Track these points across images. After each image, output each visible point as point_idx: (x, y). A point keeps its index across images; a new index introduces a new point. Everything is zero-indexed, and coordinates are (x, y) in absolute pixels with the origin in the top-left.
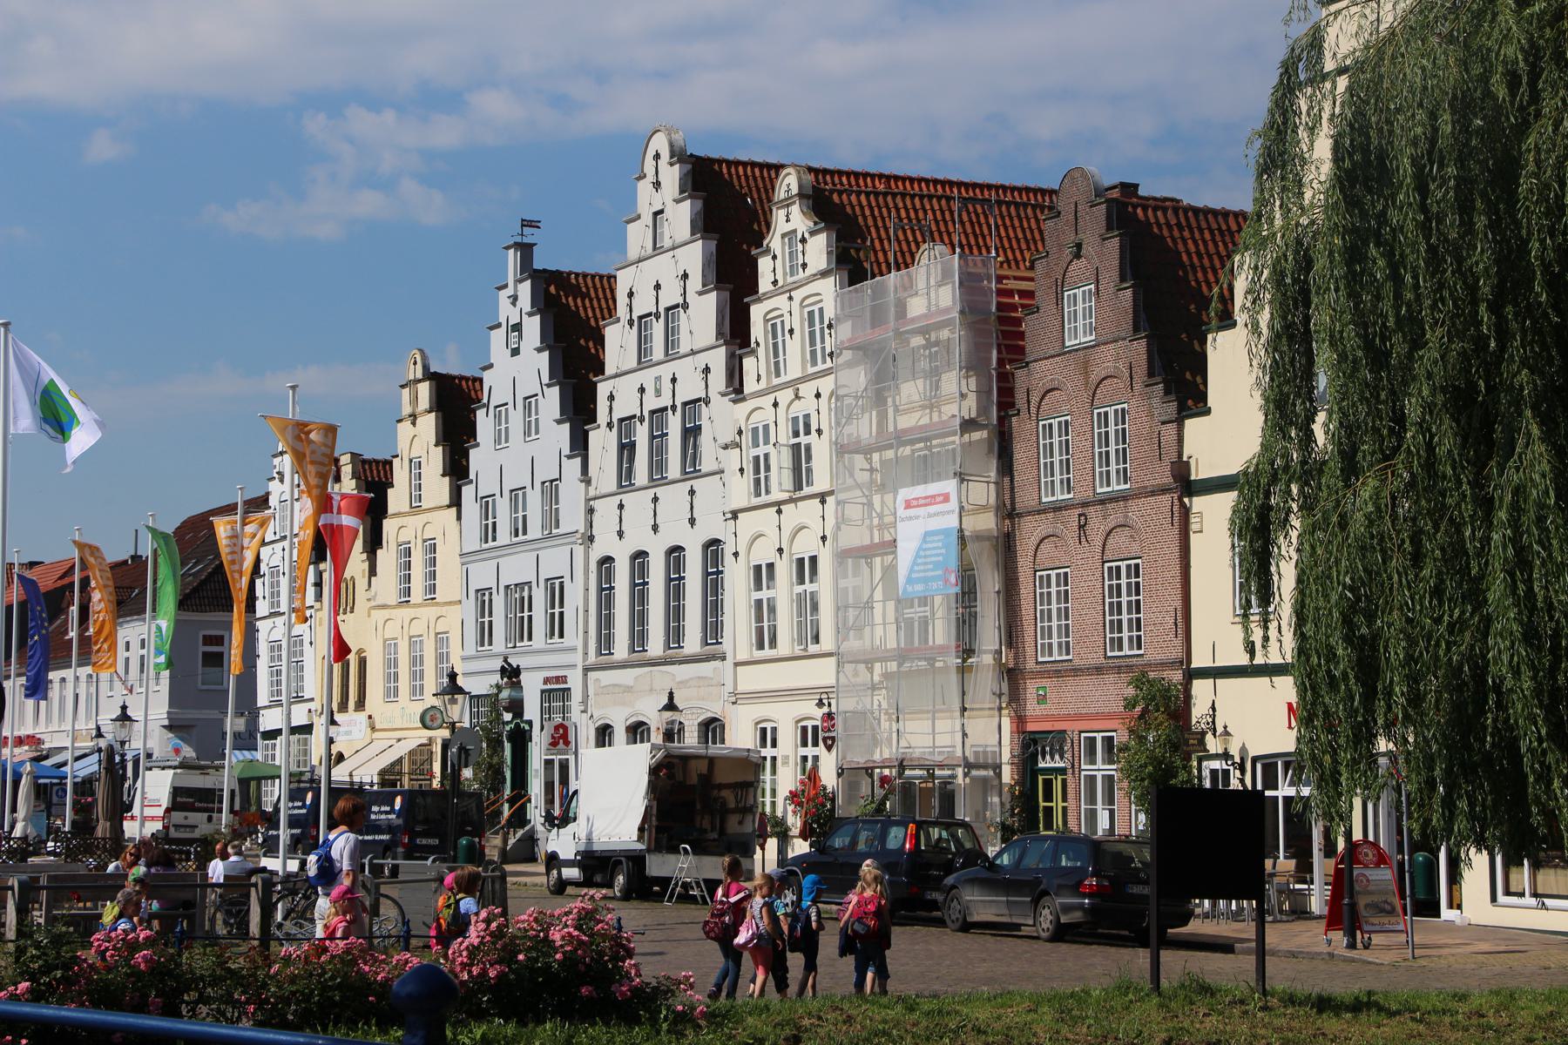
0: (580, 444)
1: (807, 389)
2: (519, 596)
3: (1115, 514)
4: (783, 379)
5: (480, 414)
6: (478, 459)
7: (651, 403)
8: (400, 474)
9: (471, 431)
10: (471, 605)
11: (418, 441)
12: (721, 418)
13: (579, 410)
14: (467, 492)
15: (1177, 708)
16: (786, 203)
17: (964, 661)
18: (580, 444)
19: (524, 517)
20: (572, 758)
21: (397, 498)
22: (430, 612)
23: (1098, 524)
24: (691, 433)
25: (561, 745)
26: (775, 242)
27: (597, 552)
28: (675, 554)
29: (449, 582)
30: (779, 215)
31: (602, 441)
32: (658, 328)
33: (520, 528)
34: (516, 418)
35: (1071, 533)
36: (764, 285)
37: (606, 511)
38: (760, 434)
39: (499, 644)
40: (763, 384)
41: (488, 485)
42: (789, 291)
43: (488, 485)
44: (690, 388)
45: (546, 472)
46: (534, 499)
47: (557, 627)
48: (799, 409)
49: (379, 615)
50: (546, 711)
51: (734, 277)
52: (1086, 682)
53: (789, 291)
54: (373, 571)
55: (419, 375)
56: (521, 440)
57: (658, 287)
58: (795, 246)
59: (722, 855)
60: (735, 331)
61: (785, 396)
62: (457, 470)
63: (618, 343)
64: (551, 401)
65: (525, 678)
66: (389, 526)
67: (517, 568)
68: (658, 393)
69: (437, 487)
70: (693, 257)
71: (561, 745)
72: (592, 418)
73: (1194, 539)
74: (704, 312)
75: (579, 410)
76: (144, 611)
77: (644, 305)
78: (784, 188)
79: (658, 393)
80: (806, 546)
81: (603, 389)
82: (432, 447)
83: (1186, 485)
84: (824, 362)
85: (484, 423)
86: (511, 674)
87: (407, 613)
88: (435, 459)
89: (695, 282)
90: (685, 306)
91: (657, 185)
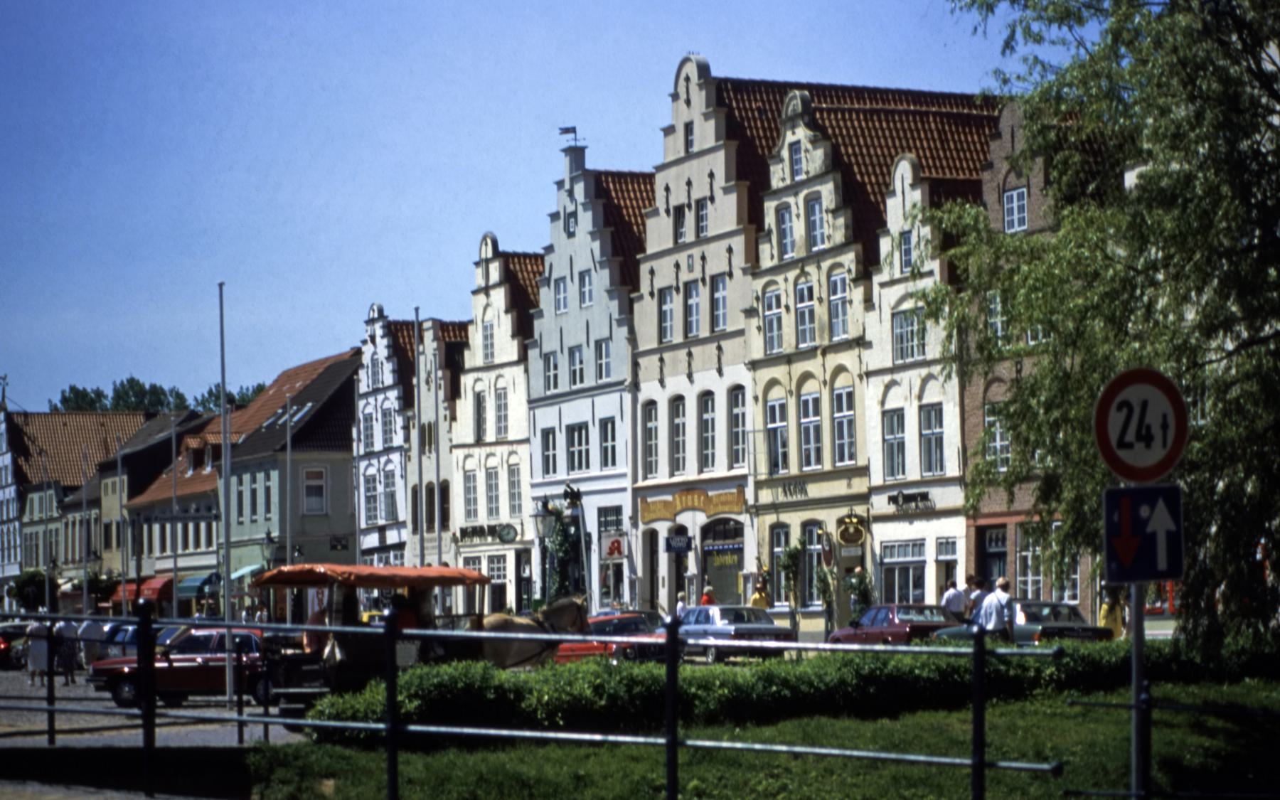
0: (627, 315)
2: (577, 431)
4: (770, 519)
6: (541, 326)
7: (685, 276)
8: (476, 337)
10: (537, 441)
11: (494, 312)
13: (626, 279)
14: (533, 353)
16: (792, 122)
17: (1232, 144)
18: (627, 315)
19: (581, 370)
20: (625, 562)
21: (473, 357)
22: (502, 450)
25: (616, 555)
27: (642, 397)
28: (706, 398)
29: (518, 424)
31: (646, 311)
32: (690, 217)
33: (575, 376)
34: (573, 289)
36: (776, 183)
37: (649, 365)
39: (562, 474)
40: (775, 262)
41: (550, 344)
43: (550, 344)
44: (716, 265)
45: (600, 332)
46: (589, 354)
47: (608, 457)
49: (460, 453)
50: (603, 525)
51: (750, 174)
54: (453, 418)
55: (490, 255)
56: (578, 312)
57: (689, 183)
58: (800, 153)
60: (752, 218)
62: (524, 330)
63: (658, 233)
64: (601, 279)
65: (585, 500)
66: (467, 381)
67: (576, 411)
68: (691, 268)
69: (507, 348)
70: (719, 162)
71: (616, 555)
72: (636, 287)
74: (725, 213)
75: (626, 279)
77: (678, 198)
78: (791, 108)
79: (691, 268)
81: (644, 269)
82: (502, 314)
84: (823, 242)
85: (546, 297)
86: (574, 497)
87: (483, 451)
88: (504, 325)
89: (720, 181)
90: (712, 199)
91: (688, 102)
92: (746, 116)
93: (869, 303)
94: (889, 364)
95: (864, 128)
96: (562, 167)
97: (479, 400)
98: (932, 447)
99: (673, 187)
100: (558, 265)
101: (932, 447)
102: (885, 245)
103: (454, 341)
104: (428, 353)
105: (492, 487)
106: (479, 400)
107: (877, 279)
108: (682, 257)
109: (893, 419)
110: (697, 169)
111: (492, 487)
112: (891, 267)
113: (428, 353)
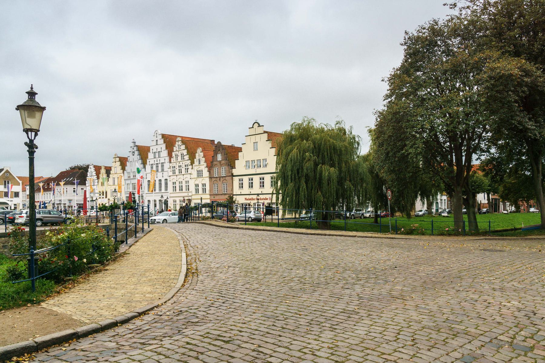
1: (181, 163)
3: (224, 178)
5: (127, 163)
7: (156, 162)
9: (147, 157)
12: (167, 165)
15: (232, 198)
23: (222, 179)
24: (163, 166)
26: (176, 146)
30: (177, 143)
32: (157, 154)
35: (218, 181)
36: (175, 150)
38: (174, 167)
42: (178, 151)
46: (160, 165)
48: (180, 165)
52: (220, 196)
53: (178, 151)
59: (378, 134)
61: (178, 163)
63: (151, 155)
73: (234, 182)
74: (165, 153)
76: (40, 191)
80: (180, 180)
81: (148, 161)
83: (233, 176)
92: (169, 141)
93: (192, 168)
94: (36, 175)
95: (192, 145)
96: (132, 145)
97: (114, 178)
98: (204, 190)
99: (153, 149)
100: (130, 159)
101: (204, 190)
102: (195, 160)
103: (108, 171)
104: (103, 171)
105: (160, 184)
106: (114, 178)
107: (194, 165)
108: (155, 159)
109: (197, 185)
110: (159, 147)
111: (160, 184)
112: (196, 162)
113: (103, 171)
